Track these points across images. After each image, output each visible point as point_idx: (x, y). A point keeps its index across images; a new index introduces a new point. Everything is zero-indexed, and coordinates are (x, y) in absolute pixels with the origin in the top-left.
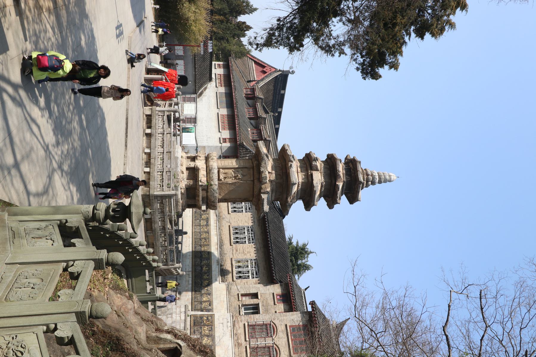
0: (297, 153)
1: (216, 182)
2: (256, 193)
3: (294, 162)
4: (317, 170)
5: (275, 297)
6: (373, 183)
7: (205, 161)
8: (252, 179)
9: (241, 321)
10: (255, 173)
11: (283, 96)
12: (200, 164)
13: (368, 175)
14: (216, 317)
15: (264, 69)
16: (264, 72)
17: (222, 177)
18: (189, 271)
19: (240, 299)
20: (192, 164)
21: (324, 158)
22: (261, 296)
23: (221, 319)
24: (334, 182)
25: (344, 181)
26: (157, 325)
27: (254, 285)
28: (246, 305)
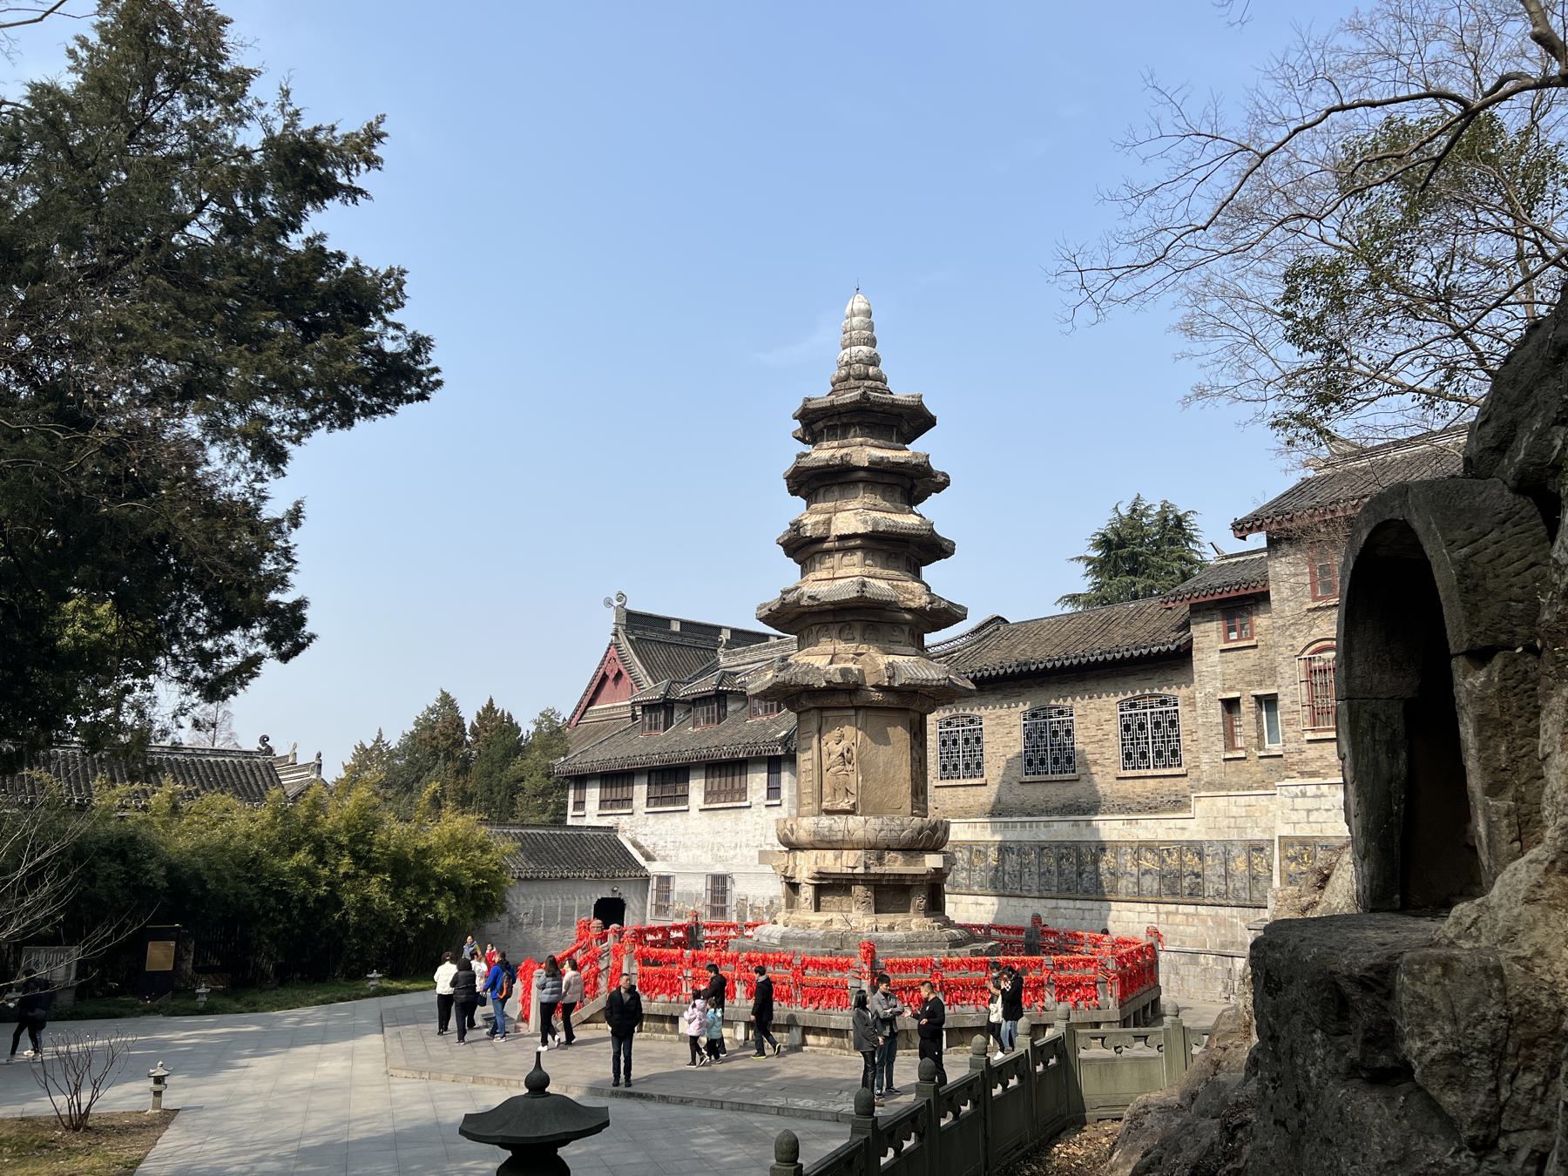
0: (782, 577)
1: (857, 826)
2: (893, 700)
3: (805, 589)
4: (828, 522)
5: (1233, 645)
6: (874, 361)
7: (798, 853)
8: (852, 712)
9: (1301, 752)
10: (834, 704)
11: (685, 624)
12: (806, 866)
13: (847, 378)
14: (1287, 831)
15: (612, 676)
16: (619, 675)
17: (845, 805)
18: (1158, 913)
19: (1242, 754)
20: (807, 892)
21: (799, 502)
22: (1231, 689)
23: (1294, 817)
24: (862, 474)
25: (867, 439)
26: (1231, 1032)
27: (1200, 711)
28: (1260, 737)
